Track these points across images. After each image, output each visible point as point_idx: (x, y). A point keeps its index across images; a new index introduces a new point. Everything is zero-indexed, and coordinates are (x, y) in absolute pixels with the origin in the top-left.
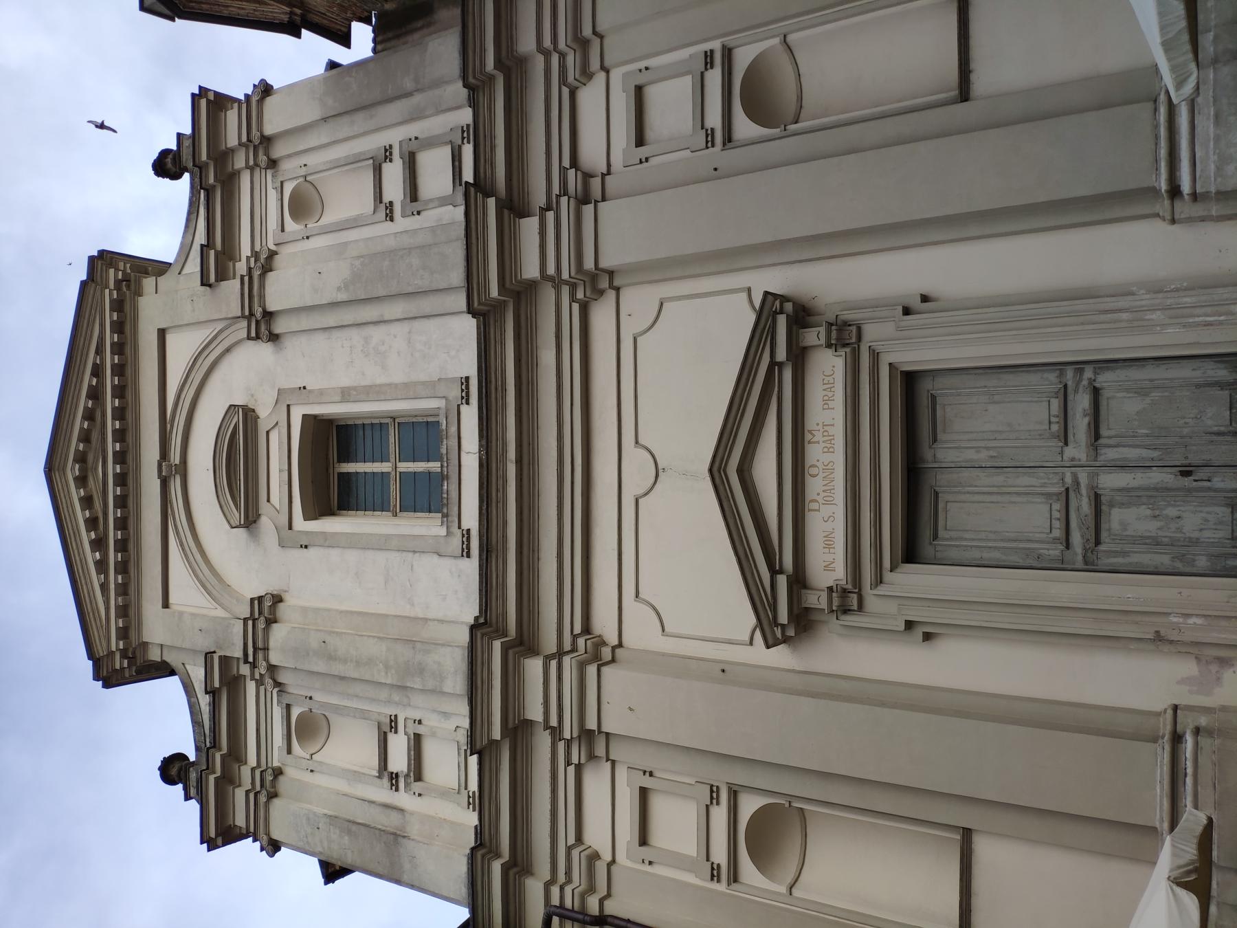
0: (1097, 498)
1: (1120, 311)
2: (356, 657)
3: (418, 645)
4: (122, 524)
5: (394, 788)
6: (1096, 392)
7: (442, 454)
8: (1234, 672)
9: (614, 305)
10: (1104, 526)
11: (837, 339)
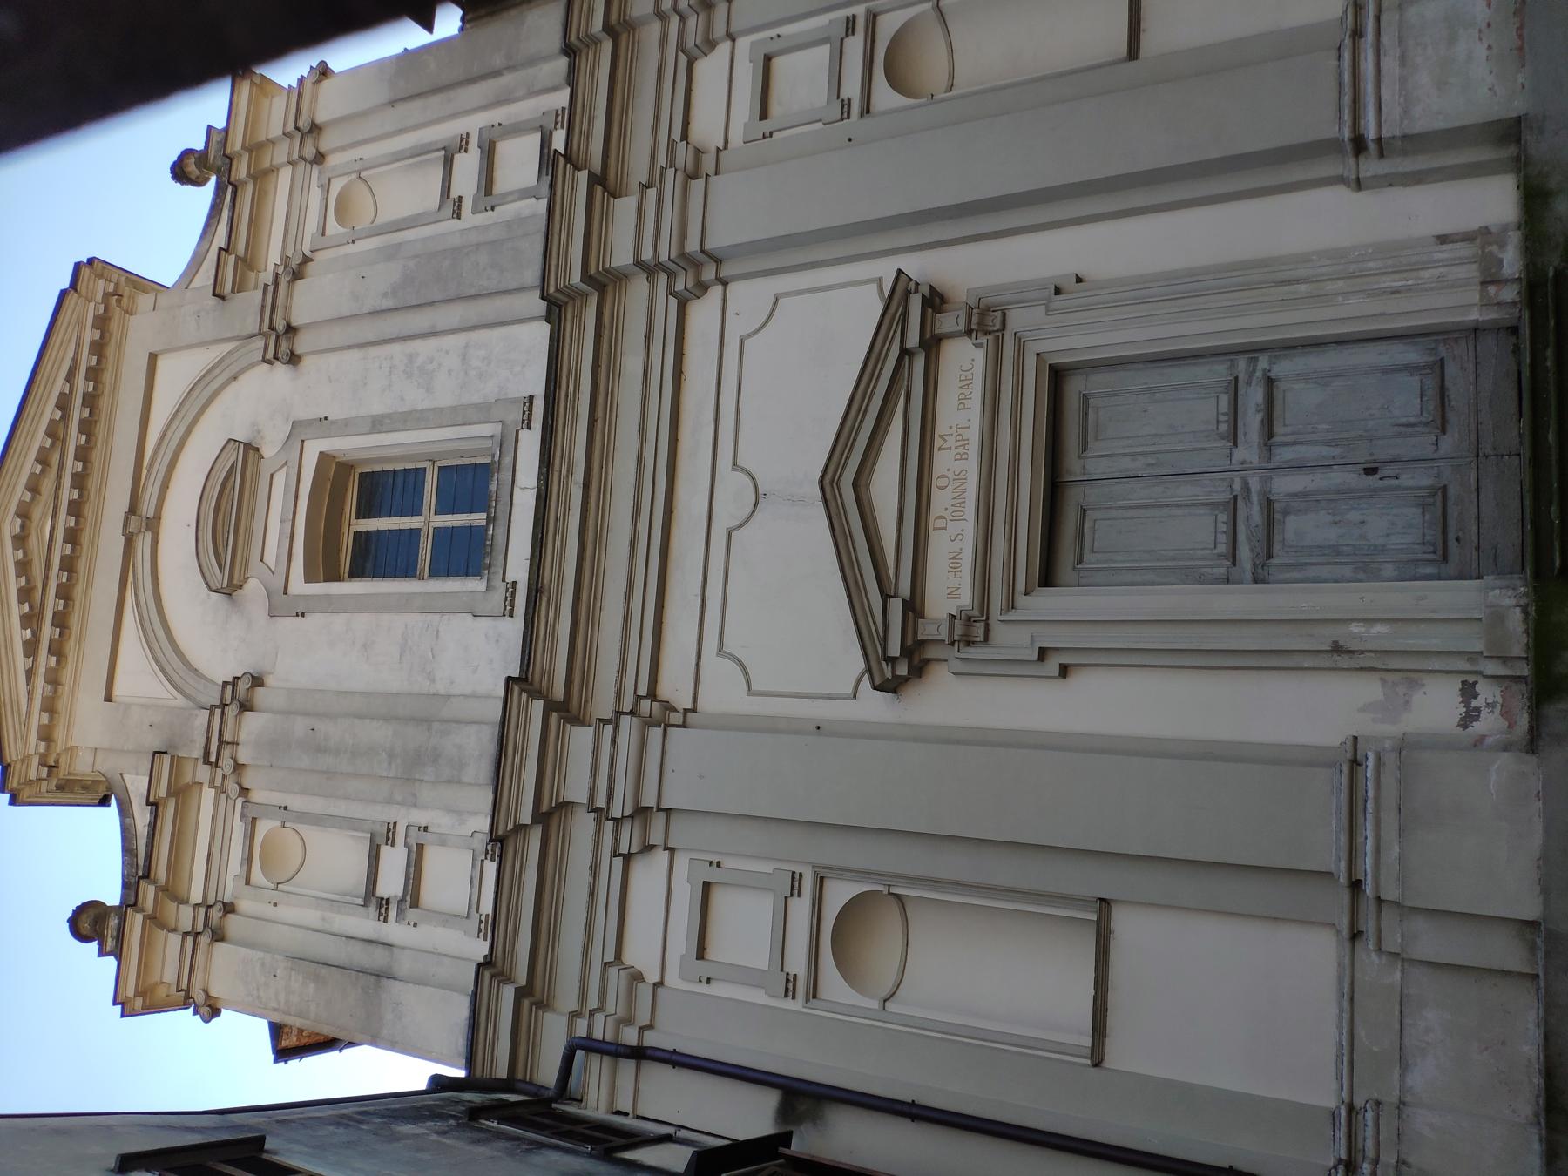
0: (1268, 505)
1: (1298, 281)
2: (353, 745)
3: (436, 725)
4: (65, 593)
5: (382, 918)
6: (1270, 383)
7: (491, 492)
8: (1425, 693)
9: (720, 302)
10: (1277, 538)
11: (979, 324)
